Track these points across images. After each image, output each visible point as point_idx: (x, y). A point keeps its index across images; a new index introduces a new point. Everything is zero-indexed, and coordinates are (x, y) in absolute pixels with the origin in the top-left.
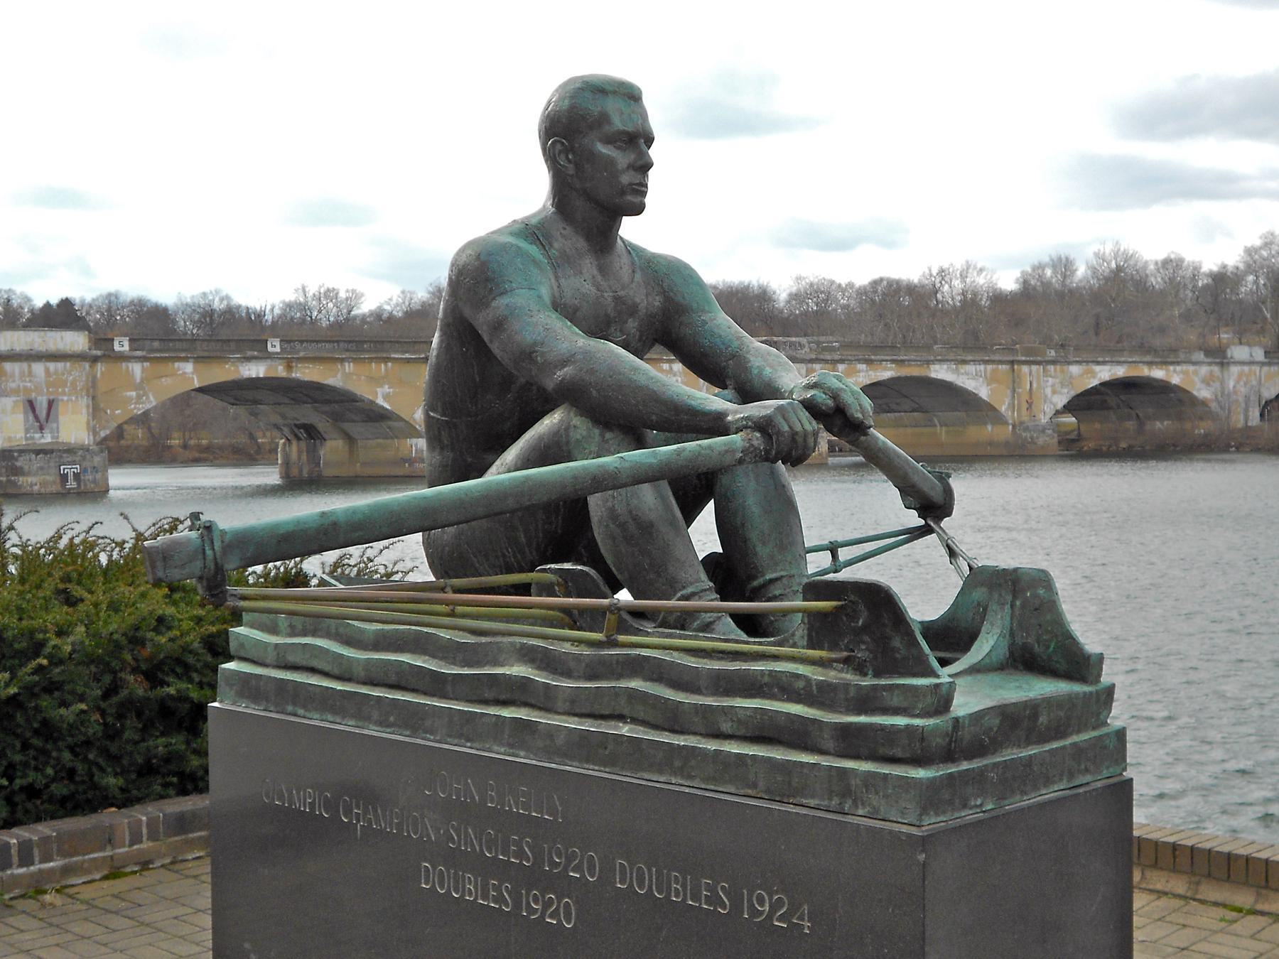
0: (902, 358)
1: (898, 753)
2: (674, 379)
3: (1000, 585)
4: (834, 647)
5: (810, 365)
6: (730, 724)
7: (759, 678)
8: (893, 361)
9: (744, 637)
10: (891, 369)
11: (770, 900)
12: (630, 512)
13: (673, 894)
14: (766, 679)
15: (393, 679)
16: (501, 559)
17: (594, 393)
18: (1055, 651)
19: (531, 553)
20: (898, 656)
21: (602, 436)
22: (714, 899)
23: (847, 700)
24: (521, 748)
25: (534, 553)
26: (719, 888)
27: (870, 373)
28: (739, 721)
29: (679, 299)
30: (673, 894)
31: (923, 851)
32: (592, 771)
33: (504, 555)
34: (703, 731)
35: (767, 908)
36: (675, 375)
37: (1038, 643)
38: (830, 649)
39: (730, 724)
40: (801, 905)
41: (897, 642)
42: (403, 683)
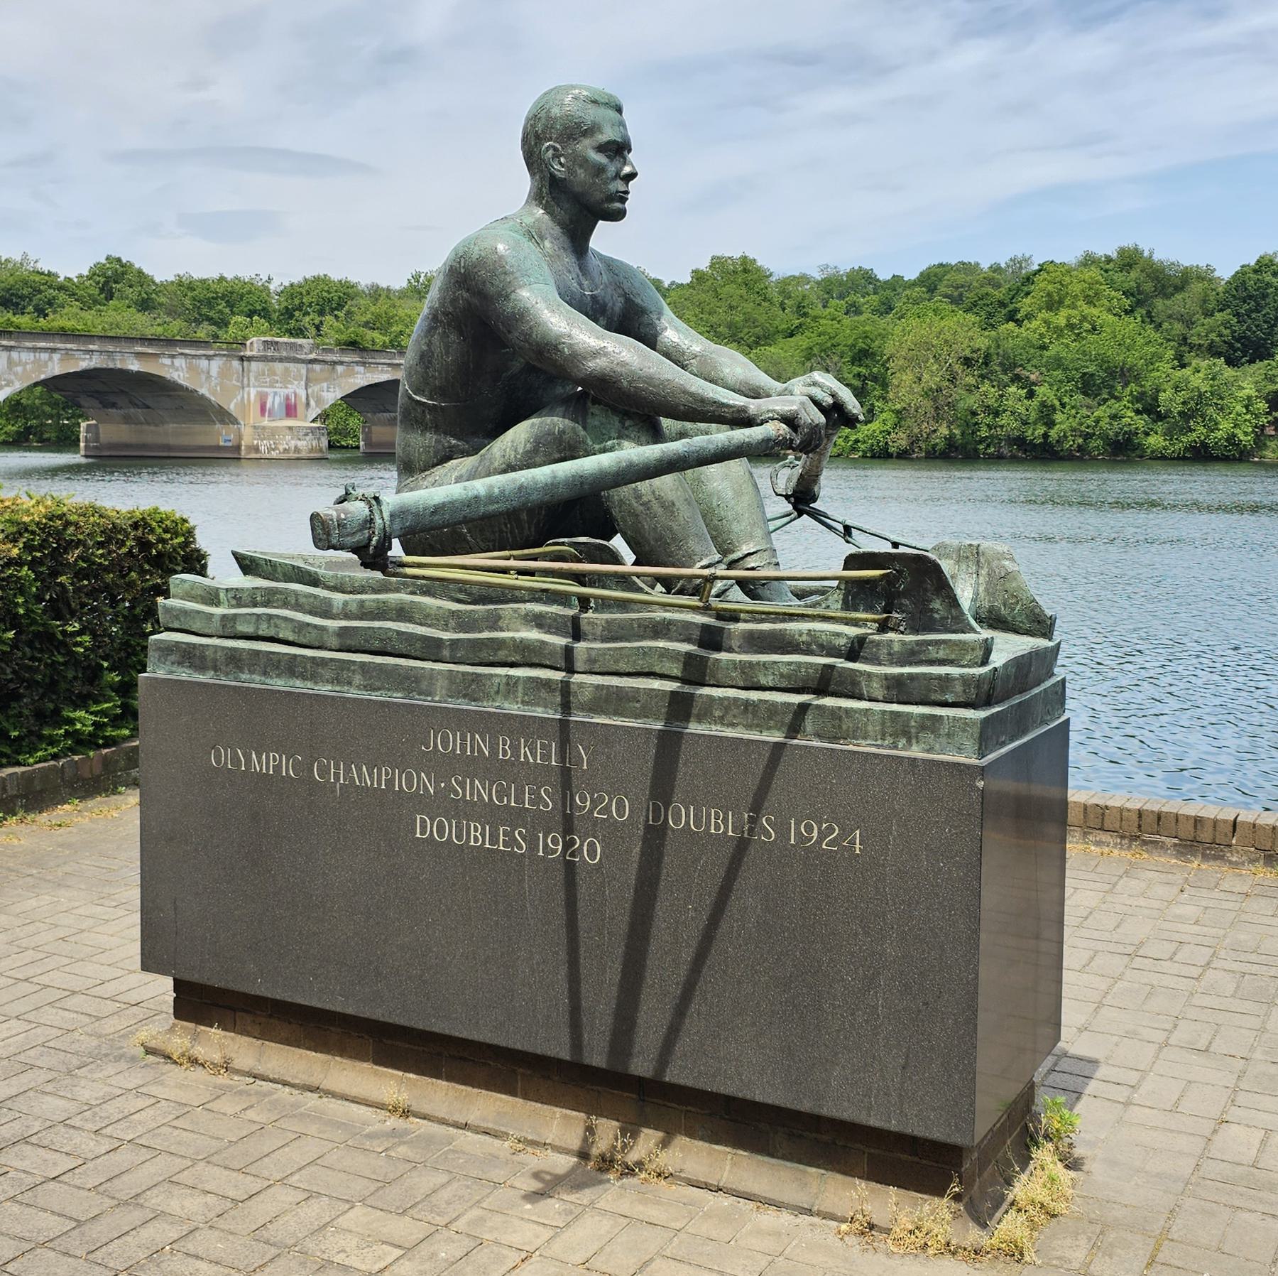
0: (397, 362)
1: (950, 698)
2: (177, 373)
3: (967, 558)
4: (869, 609)
5: (310, 366)
6: (772, 677)
7: (797, 636)
8: (389, 365)
9: (747, 599)
10: (387, 372)
11: (819, 829)
12: (653, 492)
13: (713, 827)
14: (804, 638)
15: (377, 645)
16: (497, 535)
17: (625, 384)
18: (1020, 614)
19: (529, 528)
20: (936, 616)
21: (623, 423)
22: (511, 842)
23: (889, 654)
24: (538, 705)
25: (533, 529)
26: (516, 832)
27: (368, 375)
28: (782, 675)
29: (638, 301)
30: (713, 827)
31: (983, 779)
32: (620, 721)
33: (501, 531)
34: (741, 684)
35: (560, 847)
36: (177, 370)
37: (1005, 606)
38: (866, 611)
39: (772, 677)
40: (853, 831)
41: (937, 604)
42: (389, 649)
